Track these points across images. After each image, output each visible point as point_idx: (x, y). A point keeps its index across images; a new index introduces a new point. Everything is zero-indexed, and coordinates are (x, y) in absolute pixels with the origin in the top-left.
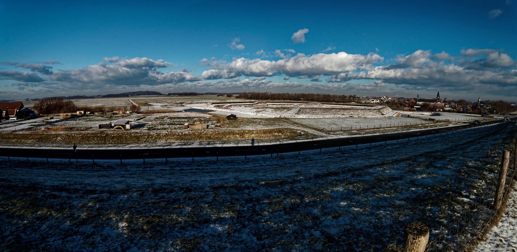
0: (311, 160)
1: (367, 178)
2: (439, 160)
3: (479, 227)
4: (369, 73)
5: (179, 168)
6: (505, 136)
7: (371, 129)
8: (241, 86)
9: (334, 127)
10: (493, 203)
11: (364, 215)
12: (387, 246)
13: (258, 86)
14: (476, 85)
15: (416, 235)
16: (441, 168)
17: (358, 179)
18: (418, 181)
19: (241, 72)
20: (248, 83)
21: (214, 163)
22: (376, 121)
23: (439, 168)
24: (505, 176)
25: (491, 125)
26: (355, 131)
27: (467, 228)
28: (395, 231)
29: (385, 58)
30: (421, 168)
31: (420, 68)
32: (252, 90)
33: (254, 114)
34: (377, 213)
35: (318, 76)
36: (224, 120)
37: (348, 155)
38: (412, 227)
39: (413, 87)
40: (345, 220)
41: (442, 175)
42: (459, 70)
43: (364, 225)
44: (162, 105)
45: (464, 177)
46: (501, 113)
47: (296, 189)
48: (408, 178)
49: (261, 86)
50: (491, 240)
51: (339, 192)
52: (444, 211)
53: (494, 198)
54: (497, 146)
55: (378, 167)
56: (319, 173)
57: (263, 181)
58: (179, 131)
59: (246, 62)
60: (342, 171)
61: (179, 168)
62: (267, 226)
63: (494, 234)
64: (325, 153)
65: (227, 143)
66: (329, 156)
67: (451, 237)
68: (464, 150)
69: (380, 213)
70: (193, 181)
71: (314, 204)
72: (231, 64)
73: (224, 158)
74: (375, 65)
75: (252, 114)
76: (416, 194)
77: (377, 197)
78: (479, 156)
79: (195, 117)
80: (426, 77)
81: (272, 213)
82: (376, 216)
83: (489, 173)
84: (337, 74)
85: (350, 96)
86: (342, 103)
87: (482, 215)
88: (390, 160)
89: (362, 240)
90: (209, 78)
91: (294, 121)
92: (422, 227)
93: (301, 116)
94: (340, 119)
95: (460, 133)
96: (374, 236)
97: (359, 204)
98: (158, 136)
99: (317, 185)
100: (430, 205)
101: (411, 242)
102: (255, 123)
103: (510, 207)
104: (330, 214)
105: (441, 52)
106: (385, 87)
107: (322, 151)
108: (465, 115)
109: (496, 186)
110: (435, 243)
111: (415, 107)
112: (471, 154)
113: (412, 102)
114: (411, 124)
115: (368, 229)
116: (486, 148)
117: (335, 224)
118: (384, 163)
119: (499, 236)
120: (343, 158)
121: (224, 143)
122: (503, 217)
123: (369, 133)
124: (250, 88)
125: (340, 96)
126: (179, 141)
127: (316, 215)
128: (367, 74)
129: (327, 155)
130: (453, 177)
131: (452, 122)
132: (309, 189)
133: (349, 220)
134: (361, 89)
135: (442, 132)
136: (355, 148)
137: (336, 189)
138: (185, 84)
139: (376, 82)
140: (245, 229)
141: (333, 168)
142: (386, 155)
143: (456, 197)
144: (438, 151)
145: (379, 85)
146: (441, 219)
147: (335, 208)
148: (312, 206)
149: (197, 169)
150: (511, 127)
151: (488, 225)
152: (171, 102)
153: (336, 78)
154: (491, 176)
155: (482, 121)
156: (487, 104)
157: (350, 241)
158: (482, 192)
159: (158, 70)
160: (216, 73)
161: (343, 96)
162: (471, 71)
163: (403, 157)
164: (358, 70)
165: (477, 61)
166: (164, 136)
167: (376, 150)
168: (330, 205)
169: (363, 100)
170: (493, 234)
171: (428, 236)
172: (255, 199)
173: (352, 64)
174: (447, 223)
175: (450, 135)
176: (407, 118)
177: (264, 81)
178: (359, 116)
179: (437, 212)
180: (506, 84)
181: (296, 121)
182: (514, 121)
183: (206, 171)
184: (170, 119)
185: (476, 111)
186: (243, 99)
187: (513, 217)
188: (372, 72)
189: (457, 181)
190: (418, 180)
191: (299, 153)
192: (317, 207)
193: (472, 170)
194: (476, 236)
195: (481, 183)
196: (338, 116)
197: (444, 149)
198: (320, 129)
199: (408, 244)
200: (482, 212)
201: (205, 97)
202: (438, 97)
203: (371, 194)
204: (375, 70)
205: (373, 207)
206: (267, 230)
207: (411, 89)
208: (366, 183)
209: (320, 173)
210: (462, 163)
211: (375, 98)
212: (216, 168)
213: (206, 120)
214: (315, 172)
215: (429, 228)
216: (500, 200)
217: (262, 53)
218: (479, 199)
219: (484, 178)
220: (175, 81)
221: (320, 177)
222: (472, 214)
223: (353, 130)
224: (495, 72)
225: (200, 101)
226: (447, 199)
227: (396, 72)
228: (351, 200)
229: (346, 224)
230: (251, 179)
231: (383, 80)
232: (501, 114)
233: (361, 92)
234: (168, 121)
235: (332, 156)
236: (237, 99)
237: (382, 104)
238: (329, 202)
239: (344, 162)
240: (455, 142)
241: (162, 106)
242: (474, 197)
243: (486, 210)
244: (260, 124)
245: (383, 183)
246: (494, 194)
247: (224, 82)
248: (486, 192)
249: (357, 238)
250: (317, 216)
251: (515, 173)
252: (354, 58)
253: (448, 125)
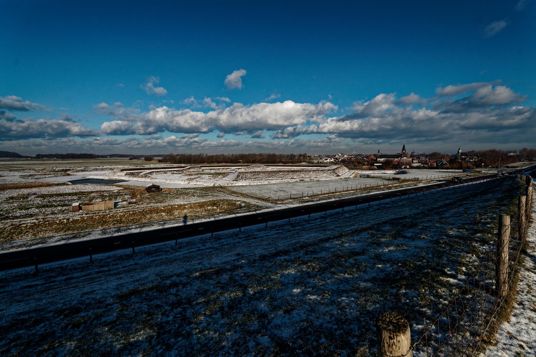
0: (255, 238)
1: (323, 254)
2: (409, 228)
3: (480, 322)
4: (321, 126)
5: (64, 278)
6: (500, 196)
7: (325, 194)
8: (164, 146)
9: (282, 195)
10: (494, 287)
11: (322, 304)
12: (357, 350)
13: (188, 145)
14: (454, 132)
15: (393, 332)
16: (412, 237)
17: (313, 256)
18: (384, 255)
19: (163, 127)
20: (175, 142)
21: (129, 257)
22: (330, 184)
23: (409, 238)
24: (506, 250)
25: (478, 182)
26: (307, 198)
27: (462, 323)
28: (364, 327)
29: (339, 107)
30: (386, 238)
31: (382, 117)
32: (181, 151)
33: (185, 183)
34: (338, 301)
35: (260, 132)
36: (143, 193)
37: (299, 228)
38: (385, 319)
39: (373, 140)
40: (299, 314)
41: (415, 247)
42: (432, 116)
43: (324, 319)
44: (23, 174)
45: (445, 249)
46: (493, 166)
47: (237, 278)
48: (373, 251)
49: (193, 146)
50: (505, 344)
51: (291, 275)
52: (425, 296)
53: (495, 280)
54: (489, 209)
55: (335, 240)
56: (265, 254)
57: (197, 271)
58: (61, 216)
59: (169, 113)
60: (293, 249)
61: (64, 278)
62: (203, 338)
63: (507, 335)
64: (272, 228)
65: (149, 226)
66: (277, 232)
67: (441, 337)
68: (442, 215)
69: (343, 300)
70: (85, 294)
71: (259, 296)
72: (148, 114)
73: (145, 248)
74: (328, 116)
75: (182, 183)
76: (384, 273)
77: (337, 278)
78: (463, 222)
79: (92, 192)
80: (389, 127)
81: (210, 316)
82: (338, 306)
83: (481, 245)
84: (282, 128)
85: (300, 155)
86: (291, 164)
87: (481, 304)
88: (349, 231)
89: (323, 343)
90: (115, 132)
91: (232, 190)
92: (399, 319)
93: (240, 183)
94: (289, 184)
95: (433, 194)
96: (338, 336)
97: (316, 290)
98: (17, 230)
99: (264, 269)
100: (404, 287)
101: (387, 343)
102: (187, 194)
103: (523, 294)
104: (281, 308)
105: (409, 94)
106: (340, 143)
107: (268, 225)
108: (440, 172)
109: (495, 263)
110: (421, 345)
111: (375, 164)
112: (450, 220)
113: (372, 160)
114: (372, 185)
115: (329, 325)
116: (473, 211)
117: (288, 321)
118: (342, 235)
119: (515, 338)
120: (294, 232)
121: (144, 226)
122: (516, 308)
123: (323, 199)
124: (178, 148)
125: (288, 155)
126: (62, 233)
127: (263, 312)
128: (318, 127)
129: (274, 230)
130: (430, 250)
131: (422, 181)
132: (253, 275)
133: (305, 313)
134: (312, 147)
135: (410, 194)
136: (307, 219)
137: (286, 272)
138: (70, 141)
139: (330, 137)
140: (171, 351)
141: (282, 245)
142: (344, 224)
143: (438, 277)
144: (406, 216)
145: (333, 140)
146: (422, 307)
147: (286, 298)
148: (258, 299)
149: (99, 272)
150: (510, 183)
151: (493, 319)
152: (44, 169)
153: (282, 133)
154: (485, 249)
155: (464, 177)
156: (470, 156)
157: (309, 347)
158: (474, 270)
159: (9, 114)
160: (125, 126)
161: (292, 155)
162: (449, 115)
163: (363, 226)
164: (308, 123)
165: (458, 100)
166: (29, 228)
167: (332, 219)
168: (280, 295)
169: (315, 159)
170: (505, 334)
171: (408, 333)
172: (186, 299)
173: (300, 116)
174: (432, 313)
175: (421, 196)
176: (366, 178)
177: (196, 139)
178: (312, 178)
179: (414, 297)
180: (501, 128)
181: (235, 189)
182: (514, 175)
183: (116, 271)
184: (42, 197)
185: (455, 165)
186: (169, 164)
187: (532, 310)
188: (324, 125)
189: (436, 255)
190: (385, 254)
191: (240, 230)
192: (264, 300)
193: (456, 241)
194: (479, 335)
195: (470, 258)
196: (286, 180)
197: (414, 214)
198: (265, 198)
199: (384, 346)
200: (479, 299)
201: (109, 161)
202: (404, 151)
203: (329, 275)
204: (327, 123)
205: (333, 292)
206: (205, 344)
207: (371, 144)
208: (322, 261)
209: (266, 253)
210: (440, 232)
211: (328, 156)
212: (131, 265)
213: (113, 196)
214: (260, 252)
215: (408, 321)
216: (504, 282)
217: (193, 101)
218: (473, 280)
219: (474, 251)
220: (49, 135)
221: (267, 258)
222: (465, 302)
223: (304, 197)
224: (485, 112)
225: (101, 167)
226: (425, 279)
227: (352, 124)
228: (305, 285)
229: (302, 319)
230: (180, 271)
232: (493, 167)
233: (312, 149)
234: (38, 201)
235: (281, 231)
236: (161, 163)
237: (337, 163)
238: (279, 290)
239: (295, 237)
240: (428, 205)
241: (23, 177)
242: (463, 277)
243: (485, 296)
244: (194, 196)
245: (343, 260)
246: (493, 273)
247: (138, 140)
248: (481, 271)
249: (317, 341)
250: (264, 313)
251: (522, 245)
252: (303, 107)
253: (417, 184)
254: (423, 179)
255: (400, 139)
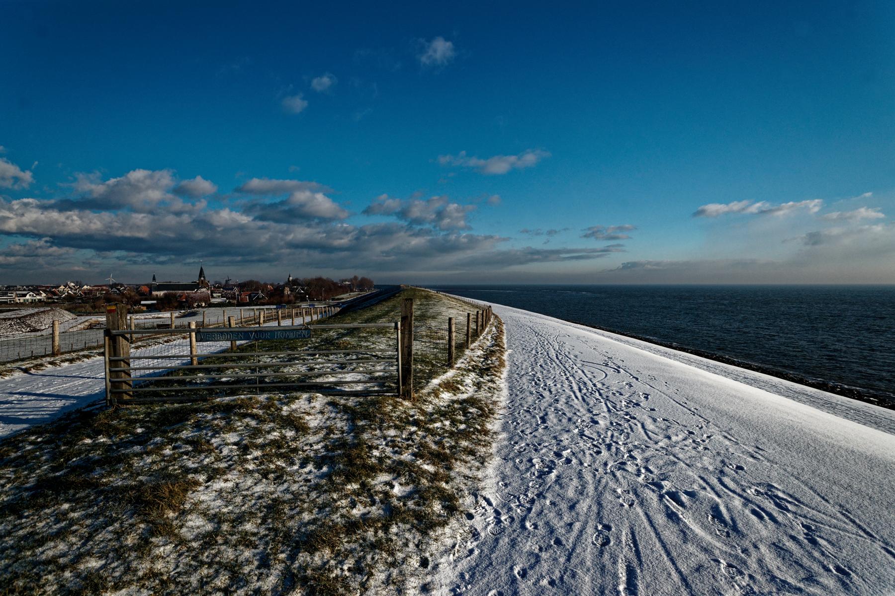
39: (147, 257)
108: (249, 309)
111: (143, 302)
202: (202, 278)
207: (144, 263)
224: (309, 226)
231: (48, 239)
237: (54, 302)
254: (211, 323)
255: (202, 256)
